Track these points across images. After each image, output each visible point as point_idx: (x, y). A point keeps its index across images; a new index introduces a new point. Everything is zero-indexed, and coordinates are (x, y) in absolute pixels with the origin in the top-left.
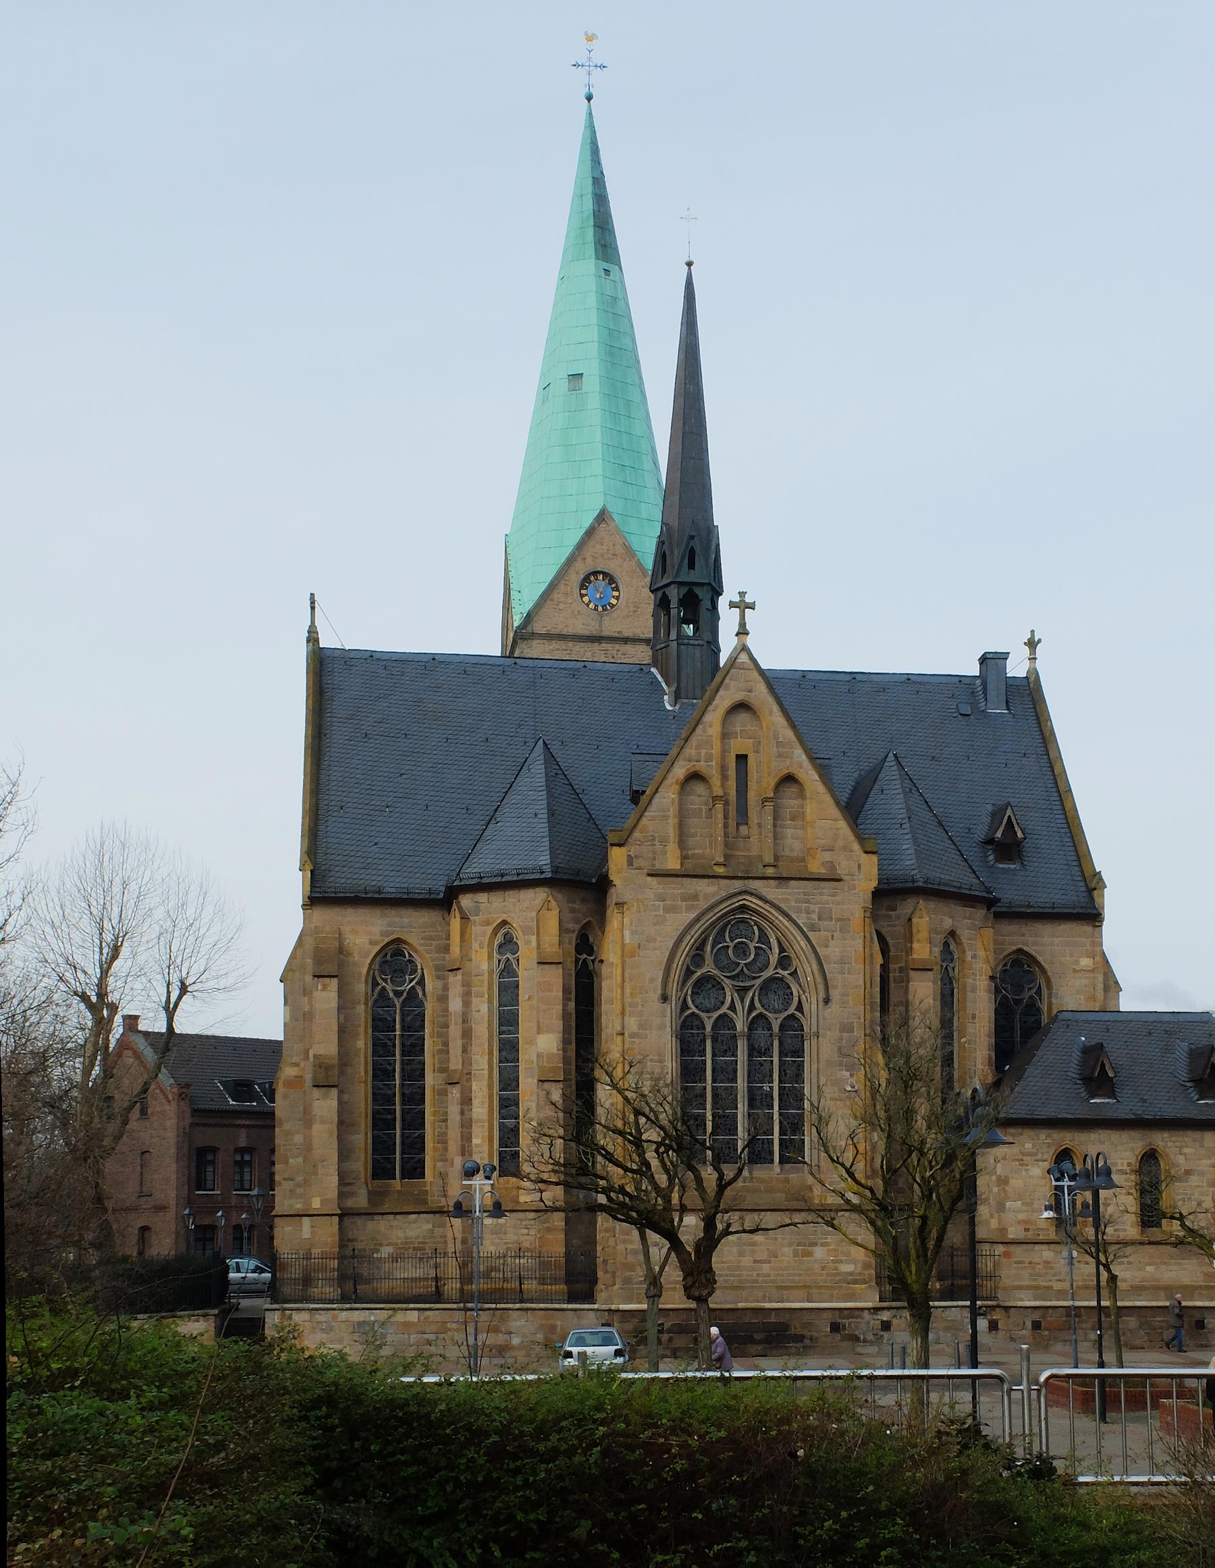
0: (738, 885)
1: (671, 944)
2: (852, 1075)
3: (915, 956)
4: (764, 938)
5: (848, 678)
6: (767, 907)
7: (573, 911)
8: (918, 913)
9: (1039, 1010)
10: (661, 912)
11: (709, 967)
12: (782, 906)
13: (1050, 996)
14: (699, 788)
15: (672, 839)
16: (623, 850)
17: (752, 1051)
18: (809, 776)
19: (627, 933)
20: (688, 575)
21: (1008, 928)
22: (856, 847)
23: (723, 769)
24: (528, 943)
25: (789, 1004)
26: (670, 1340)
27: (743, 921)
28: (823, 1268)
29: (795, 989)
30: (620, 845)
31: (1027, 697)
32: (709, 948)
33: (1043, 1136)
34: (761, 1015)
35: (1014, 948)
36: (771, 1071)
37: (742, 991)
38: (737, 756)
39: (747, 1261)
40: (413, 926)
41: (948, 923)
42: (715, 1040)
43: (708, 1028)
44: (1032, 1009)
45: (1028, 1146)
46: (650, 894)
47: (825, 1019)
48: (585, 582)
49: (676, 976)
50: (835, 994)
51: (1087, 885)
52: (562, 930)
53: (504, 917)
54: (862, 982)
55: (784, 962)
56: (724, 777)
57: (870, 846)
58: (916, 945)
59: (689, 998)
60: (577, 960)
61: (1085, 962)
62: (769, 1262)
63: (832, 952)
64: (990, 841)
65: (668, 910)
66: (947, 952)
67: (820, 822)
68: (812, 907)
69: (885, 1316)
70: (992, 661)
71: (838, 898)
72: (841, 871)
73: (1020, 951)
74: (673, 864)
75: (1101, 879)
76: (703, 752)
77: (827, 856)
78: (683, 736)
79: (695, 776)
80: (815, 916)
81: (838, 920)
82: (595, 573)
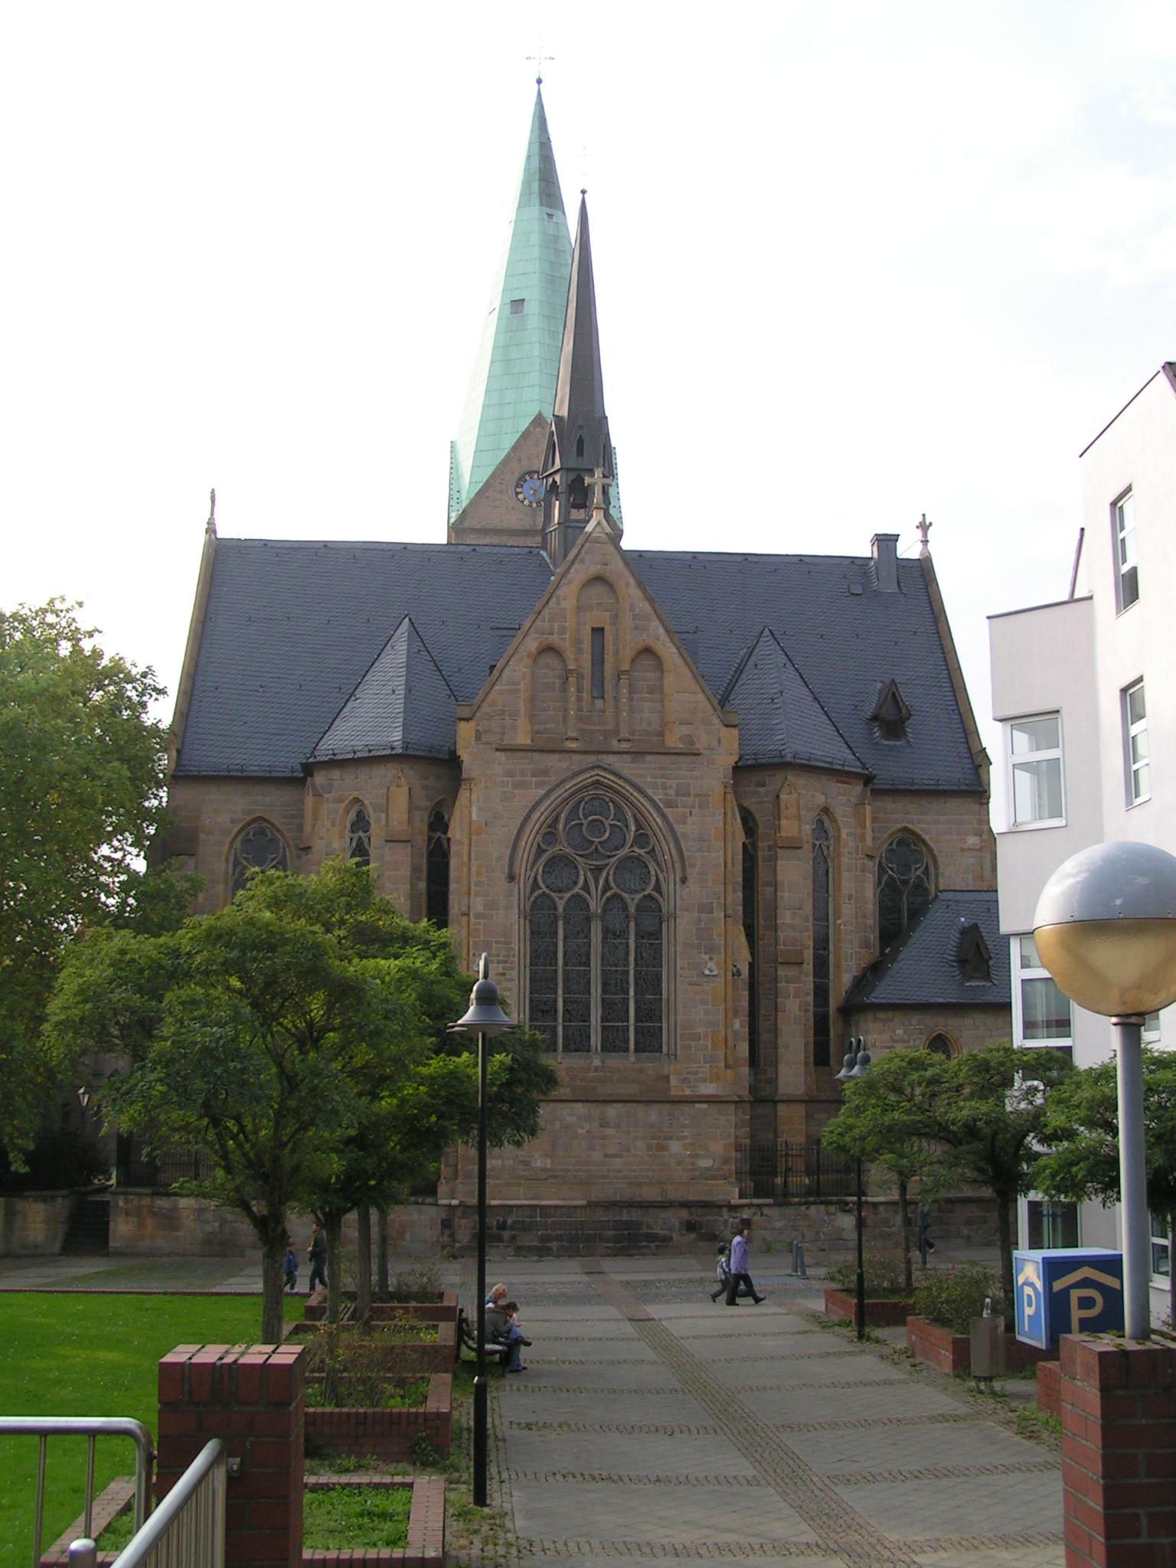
0: (591, 759)
1: (519, 823)
2: (711, 959)
3: (783, 834)
4: (620, 815)
5: (740, 559)
6: (620, 782)
7: (425, 788)
8: (786, 788)
9: (926, 890)
10: (509, 789)
11: (562, 847)
12: (637, 781)
13: (937, 875)
14: (552, 660)
15: (522, 712)
16: (472, 723)
17: (606, 932)
18: (668, 650)
19: (474, 809)
20: (572, 453)
21: (889, 804)
22: (716, 721)
23: (578, 642)
24: (378, 820)
25: (646, 883)
26: (513, 1237)
27: (597, 798)
28: (679, 1164)
29: (652, 867)
30: (467, 720)
31: (920, 577)
32: (561, 826)
33: (914, 1022)
34: (615, 896)
35: (899, 826)
36: (627, 953)
37: (597, 870)
38: (593, 629)
39: (597, 1156)
40: (270, 803)
41: (821, 799)
42: (566, 923)
43: (560, 909)
44: (920, 888)
45: (899, 1032)
46: (498, 769)
47: (682, 899)
48: (521, 482)
49: (524, 854)
50: (692, 873)
51: (973, 763)
52: (412, 808)
53: (356, 794)
54: (722, 860)
55: (641, 839)
56: (579, 651)
57: (733, 719)
58: (784, 823)
59: (539, 878)
60: (430, 839)
61: (972, 841)
62: (621, 1156)
63: (689, 828)
64: (875, 718)
65: (516, 786)
66: (820, 829)
67: (683, 694)
68: (669, 782)
69: (746, 1214)
70: (886, 542)
71: (697, 773)
72: (700, 746)
73: (906, 829)
74: (523, 738)
75: (987, 756)
76: (556, 625)
77: (685, 730)
78: (536, 609)
79: (548, 649)
80: (672, 792)
81: (697, 795)
82: (530, 473)
